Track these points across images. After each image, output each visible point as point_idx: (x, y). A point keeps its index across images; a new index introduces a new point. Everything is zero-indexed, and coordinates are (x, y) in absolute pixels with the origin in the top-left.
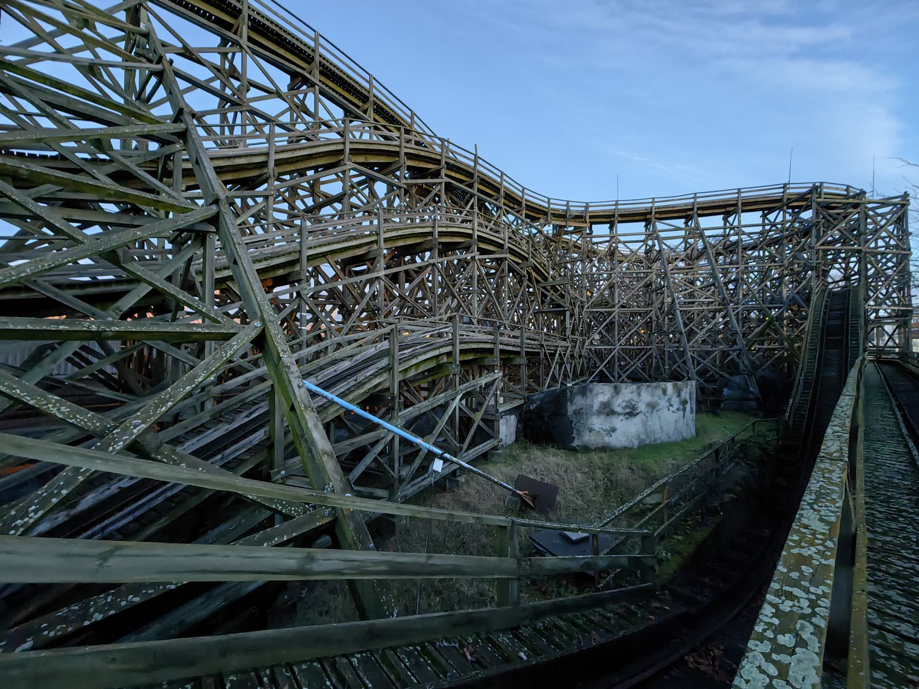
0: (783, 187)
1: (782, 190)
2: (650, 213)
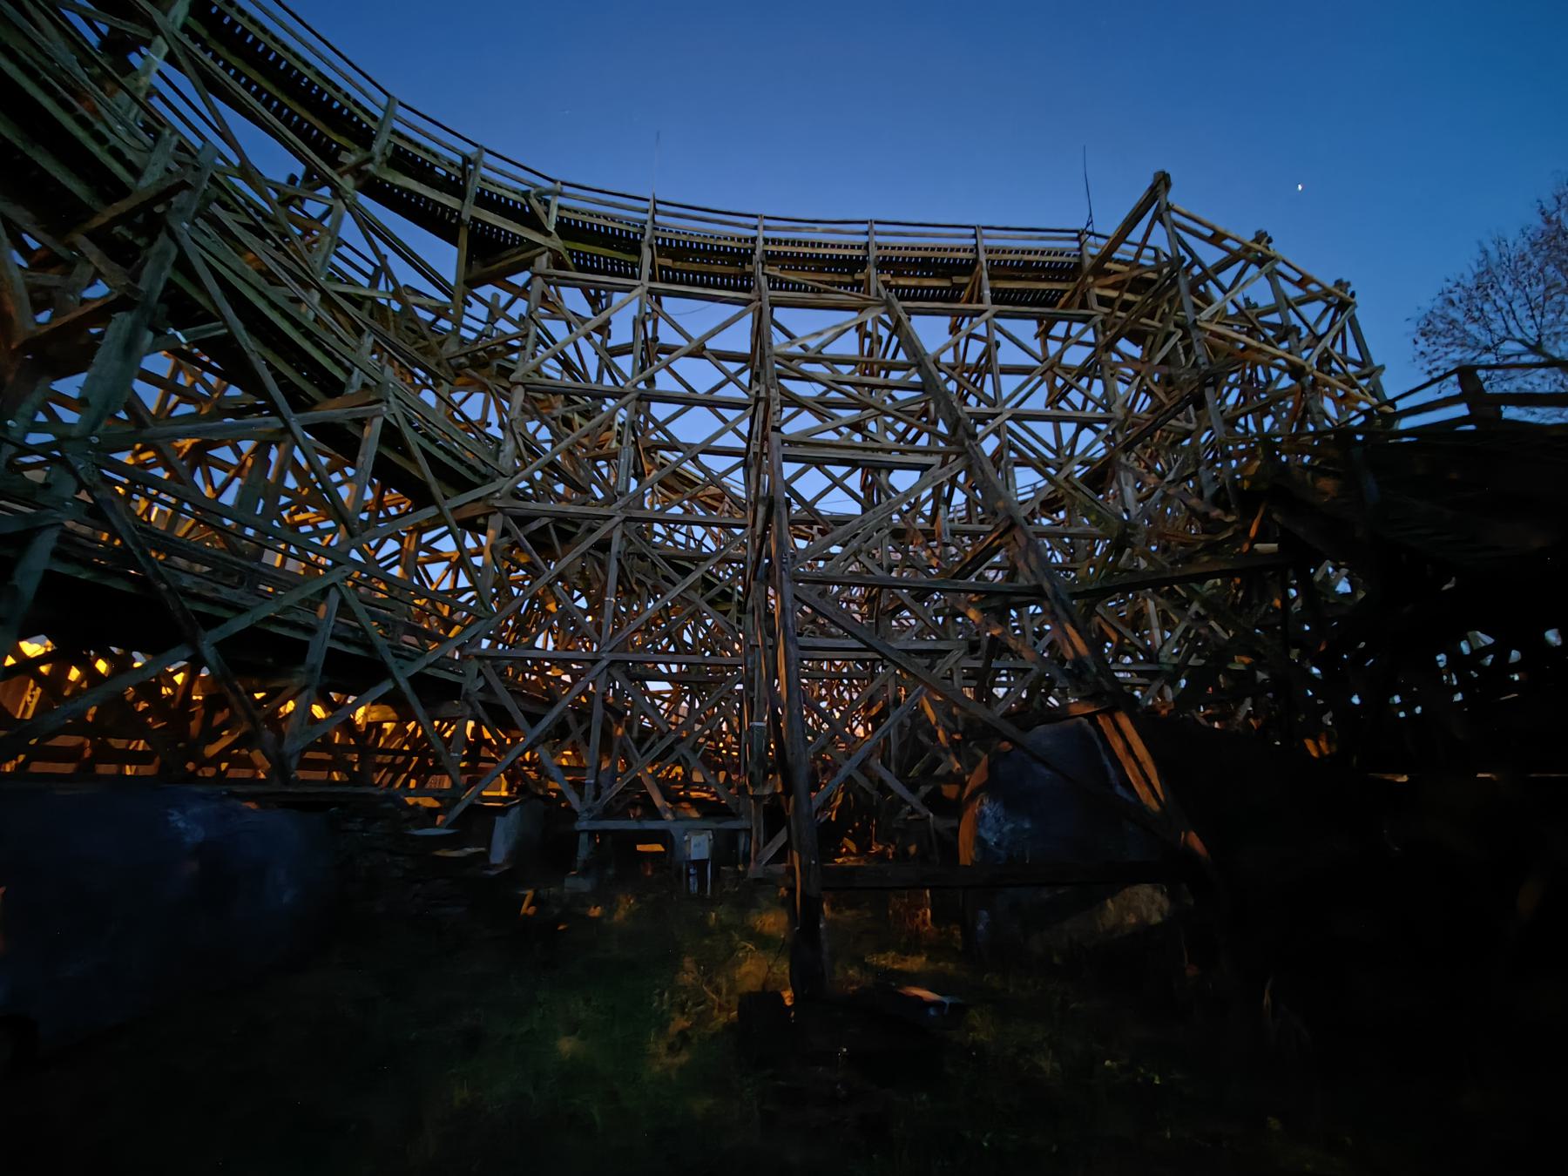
0: (1078, 239)
1: (1076, 245)
2: (747, 257)
